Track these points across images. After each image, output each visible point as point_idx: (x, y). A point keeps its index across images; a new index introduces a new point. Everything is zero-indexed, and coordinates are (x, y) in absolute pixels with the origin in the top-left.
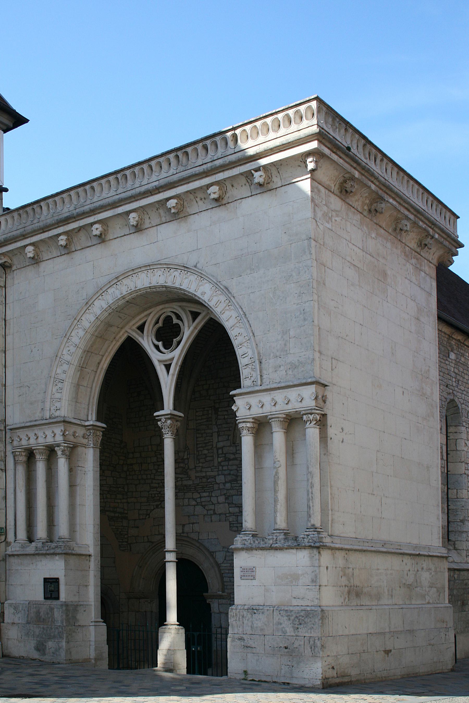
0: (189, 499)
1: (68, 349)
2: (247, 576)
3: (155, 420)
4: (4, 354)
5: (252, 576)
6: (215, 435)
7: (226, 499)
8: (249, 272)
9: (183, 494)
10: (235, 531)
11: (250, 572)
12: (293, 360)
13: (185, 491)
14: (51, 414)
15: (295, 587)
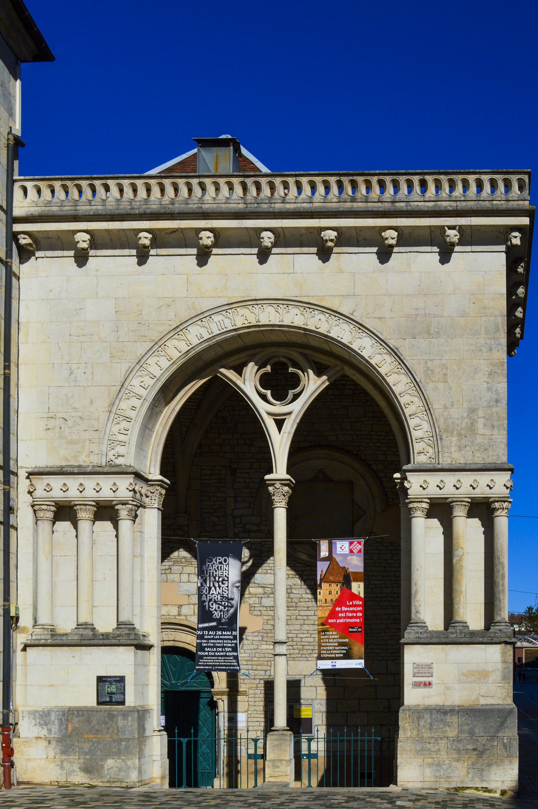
0: (189, 574)
1: (141, 379)
2: (422, 673)
3: (264, 485)
4: (17, 369)
5: (429, 673)
8: (427, 336)
9: (180, 567)
10: (257, 616)
11: (426, 669)
12: (482, 442)
13: (183, 565)
14: (108, 460)
15: (484, 684)
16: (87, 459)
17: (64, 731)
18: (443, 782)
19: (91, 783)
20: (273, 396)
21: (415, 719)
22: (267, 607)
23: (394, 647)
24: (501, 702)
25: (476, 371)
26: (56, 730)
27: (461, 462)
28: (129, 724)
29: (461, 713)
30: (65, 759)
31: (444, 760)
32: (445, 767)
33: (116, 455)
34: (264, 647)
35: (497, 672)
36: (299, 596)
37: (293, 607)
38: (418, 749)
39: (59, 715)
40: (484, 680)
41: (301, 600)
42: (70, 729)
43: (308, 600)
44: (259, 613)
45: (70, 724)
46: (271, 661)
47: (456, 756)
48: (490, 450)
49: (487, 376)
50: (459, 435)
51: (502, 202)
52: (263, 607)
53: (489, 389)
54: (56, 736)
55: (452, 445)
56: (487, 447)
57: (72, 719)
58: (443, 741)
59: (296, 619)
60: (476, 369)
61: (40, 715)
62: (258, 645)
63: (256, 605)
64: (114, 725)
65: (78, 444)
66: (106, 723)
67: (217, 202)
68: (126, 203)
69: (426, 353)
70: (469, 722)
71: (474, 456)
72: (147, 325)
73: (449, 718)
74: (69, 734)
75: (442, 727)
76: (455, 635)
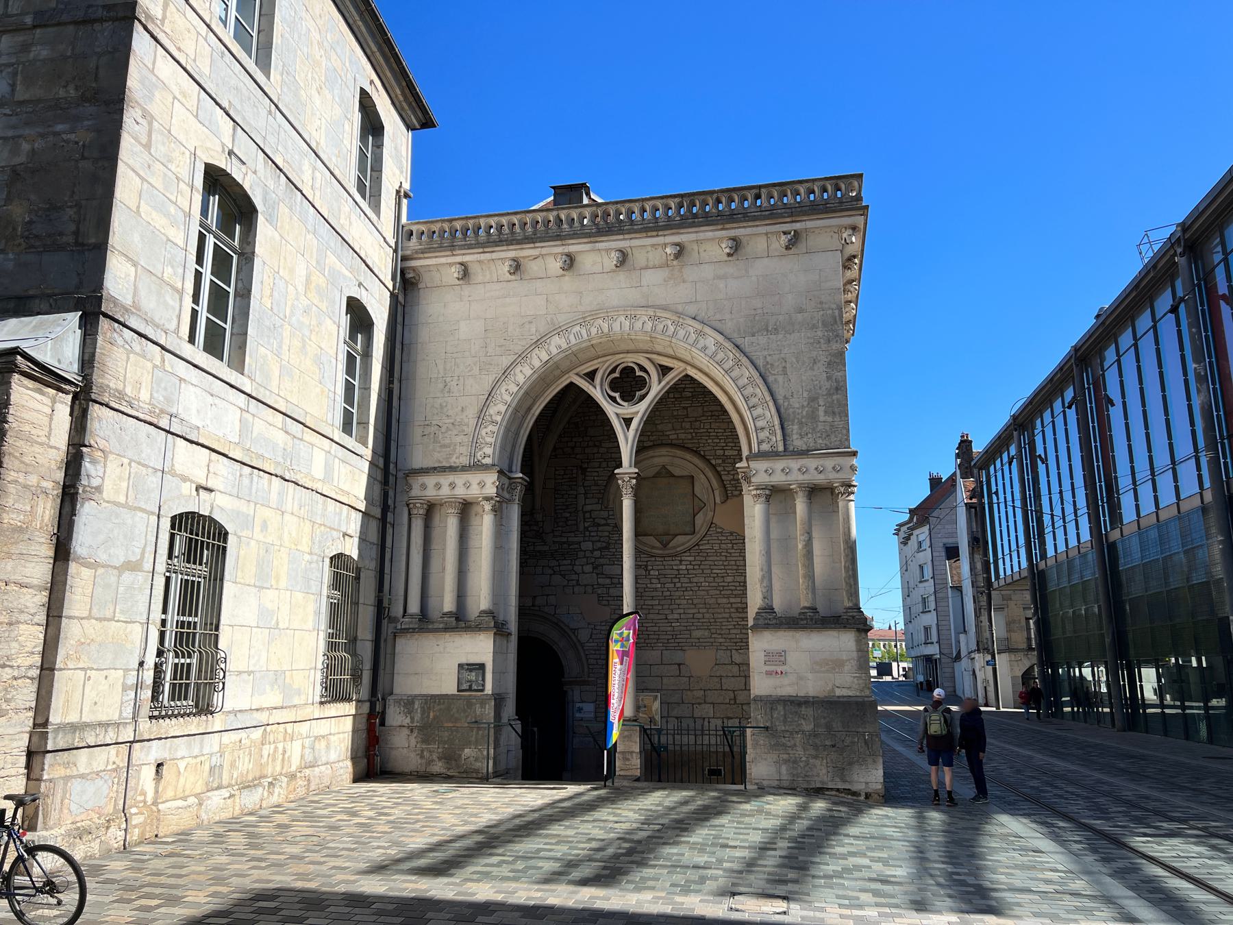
6: (581, 498)
8: (765, 333)
16: (457, 461)
24: (858, 694)
32: (802, 764)
36: (644, 586)
47: (813, 752)
50: (801, 423)
53: (829, 378)
57: (434, 708)
66: (465, 711)
70: (825, 715)
73: (803, 710)
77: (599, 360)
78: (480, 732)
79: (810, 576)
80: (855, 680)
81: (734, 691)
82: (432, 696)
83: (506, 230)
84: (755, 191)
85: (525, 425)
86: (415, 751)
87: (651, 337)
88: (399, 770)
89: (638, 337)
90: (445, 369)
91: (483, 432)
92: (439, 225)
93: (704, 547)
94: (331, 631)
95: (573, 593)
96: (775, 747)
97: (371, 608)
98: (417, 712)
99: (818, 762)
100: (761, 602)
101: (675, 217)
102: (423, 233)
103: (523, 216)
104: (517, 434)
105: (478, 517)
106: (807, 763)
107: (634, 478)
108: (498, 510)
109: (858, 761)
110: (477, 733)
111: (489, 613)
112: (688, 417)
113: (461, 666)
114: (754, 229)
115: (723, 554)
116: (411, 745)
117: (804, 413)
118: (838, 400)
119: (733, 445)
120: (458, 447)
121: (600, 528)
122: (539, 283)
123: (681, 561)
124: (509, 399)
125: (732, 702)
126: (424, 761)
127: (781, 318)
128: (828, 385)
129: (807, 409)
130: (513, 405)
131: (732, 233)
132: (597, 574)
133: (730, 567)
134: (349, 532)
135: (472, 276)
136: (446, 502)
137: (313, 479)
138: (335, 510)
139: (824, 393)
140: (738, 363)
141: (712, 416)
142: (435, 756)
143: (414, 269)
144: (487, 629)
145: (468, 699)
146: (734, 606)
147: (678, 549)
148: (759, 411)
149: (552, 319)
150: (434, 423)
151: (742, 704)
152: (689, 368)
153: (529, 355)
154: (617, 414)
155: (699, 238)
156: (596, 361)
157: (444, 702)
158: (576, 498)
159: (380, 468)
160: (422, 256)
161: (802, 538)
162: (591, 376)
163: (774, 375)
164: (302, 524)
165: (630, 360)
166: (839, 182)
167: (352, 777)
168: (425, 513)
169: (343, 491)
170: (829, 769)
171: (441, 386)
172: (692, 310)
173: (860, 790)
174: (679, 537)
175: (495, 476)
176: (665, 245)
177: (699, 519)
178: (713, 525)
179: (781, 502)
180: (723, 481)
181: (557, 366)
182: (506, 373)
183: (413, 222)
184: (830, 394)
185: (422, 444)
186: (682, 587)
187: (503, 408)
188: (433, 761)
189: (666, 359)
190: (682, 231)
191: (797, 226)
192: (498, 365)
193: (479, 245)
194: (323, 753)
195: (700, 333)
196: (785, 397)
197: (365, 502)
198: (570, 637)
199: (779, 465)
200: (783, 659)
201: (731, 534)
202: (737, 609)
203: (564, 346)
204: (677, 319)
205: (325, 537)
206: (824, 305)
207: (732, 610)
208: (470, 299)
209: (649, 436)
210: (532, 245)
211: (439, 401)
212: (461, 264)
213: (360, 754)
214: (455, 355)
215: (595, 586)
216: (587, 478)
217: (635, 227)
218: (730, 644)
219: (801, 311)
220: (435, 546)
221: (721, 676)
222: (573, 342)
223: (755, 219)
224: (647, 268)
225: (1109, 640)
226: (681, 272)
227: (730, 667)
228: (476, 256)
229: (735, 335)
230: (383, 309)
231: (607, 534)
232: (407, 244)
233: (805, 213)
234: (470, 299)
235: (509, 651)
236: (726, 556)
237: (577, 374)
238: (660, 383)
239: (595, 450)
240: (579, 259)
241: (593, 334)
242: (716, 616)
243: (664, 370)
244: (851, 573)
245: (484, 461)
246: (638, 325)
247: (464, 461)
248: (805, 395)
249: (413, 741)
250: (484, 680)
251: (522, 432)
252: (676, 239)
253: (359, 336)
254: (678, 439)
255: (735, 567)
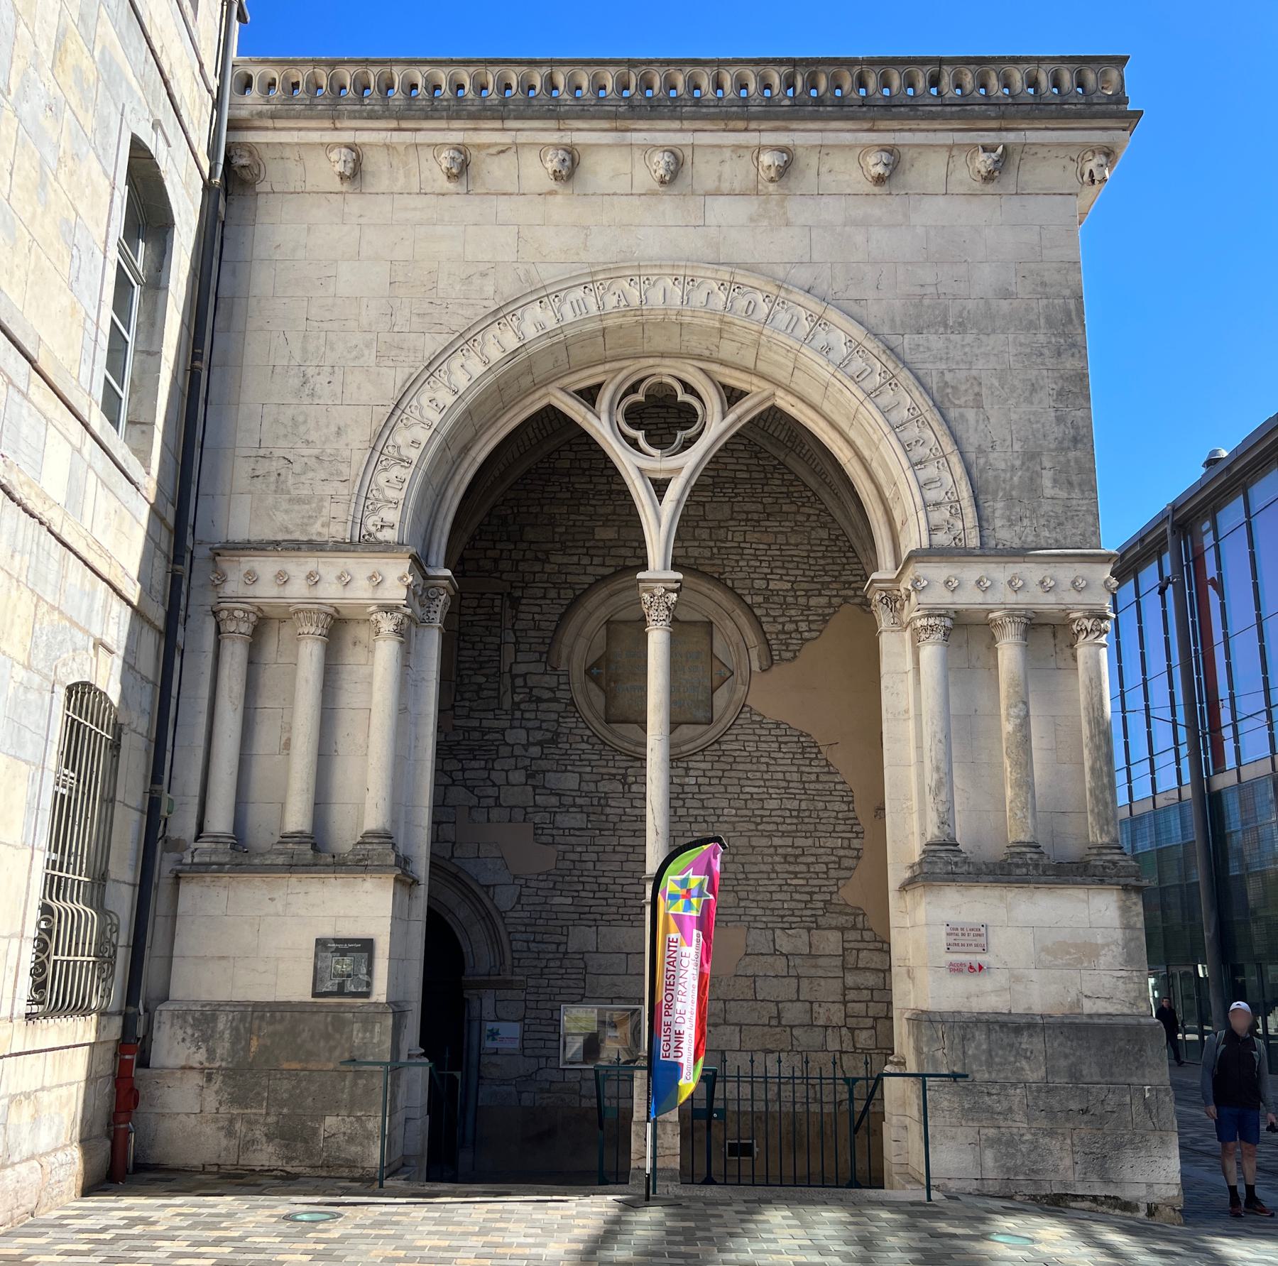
2: (963, 945)
6: (509, 651)
7: (528, 777)
8: (941, 330)
16: (325, 531)
17: (242, 1053)
18: (1023, 1182)
19: (289, 1169)
20: (648, 437)
21: (957, 1041)
22: (564, 829)
23: (786, 906)
24: (1126, 1011)
25: (1034, 389)
26: (225, 1051)
27: (1014, 546)
28: (375, 1041)
29: (1051, 1032)
30: (238, 1114)
31: (1022, 1132)
32: (1024, 1148)
33: (380, 524)
34: (557, 900)
35: (1113, 947)
36: (620, 811)
37: (609, 830)
38: (967, 1106)
39: (233, 1019)
40: (1090, 962)
41: (623, 818)
42: (253, 1050)
43: (635, 818)
44: (550, 839)
45: (255, 1038)
46: (568, 927)
47: (1045, 1124)
48: (1068, 526)
49: (1055, 397)
50: (1010, 498)
51: (1079, 106)
52: (559, 828)
53: (1060, 420)
54: (224, 1064)
55: (996, 515)
56: (1062, 519)
57: (260, 1028)
58: (1018, 1091)
59: (614, 851)
60: (1033, 385)
61: (194, 1018)
62: (546, 897)
63: (545, 826)
64: (343, 1041)
65: (309, 503)
66: (328, 1037)
67: (582, 103)
68: (424, 103)
69: (941, 359)
70: (1067, 1051)
71: (1037, 536)
72: (445, 305)
73: (1025, 1041)
74: (250, 1060)
75: (1012, 1059)
76: (1024, 870)
77: (607, 366)
78: (361, 1082)
79: (1026, 783)
80: (1120, 983)
81: (777, 1003)
82: (256, 1005)
83: (445, 91)
84: (930, 69)
85: (457, 478)
86: (216, 1121)
87: (721, 321)
88: (172, 1162)
89: (696, 321)
90: (304, 350)
91: (381, 479)
92: (308, 70)
93: (729, 747)
94: (53, 856)
95: (489, 820)
96: (969, 1114)
97: (136, 816)
98: (221, 1037)
99: (1055, 1144)
100: (936, 832)
101: (781, 100)
102: (272, 84)
103: (481, 69)
104: (441, 496)
105: (359, 649)
106: (1035, 1146)
107: (673, 591)
108: (405, 634)
109: (1131, 1142)
110: (355, 1084)
111: (385, 836)
112: (706, 520)
113: (321, 944)
114: (931, 135)
115: (763, 760)
116: (207, 1109)
117: (1016, 479)
118: (1077, 461)
119: (784, 572)
120: (326, 504)
121: (543, 706)
122: (503, 203)
123: (687, 769)
124: (436, 418)
125: (774, 1022)
126: (234, 1142)
127: (970, 305)
128: (1058, 431)
129: (1020, 473)
130: (444, 431)
131: (888, 138)
132: (535, 787)
133: (774, 783)
134: (107, 640)
135: (368, 178)
136: (297, 612)
137: (45, 498)
138: (82, 584)
139: (1052, 446)
140: (891, 381)
141: (747, 520)
142: (258, 1133)
143: (250, 148)
144: (380, 869)
145: (336, 1011)
146: (780, 851)
147: (684, 748)
148: (930, 471)
149: (527, 271)
150: (277, 453)
151: (792, 1027)
152: (780, 393)
153: (479, 337)
154: (640, 470)
155: (825, 142)
156: (600, 369)
157: (282, 1019)
158: (499, 649)
159: (166, 526)
160: (269, 123)
161: (1014, 711)
162: (589, 395)
163: (960, 407)
164: (14, 593)
165: (667, 371)
166: (1084, 67)
167: (80, 1183)
168: (249, 631)
169: (100, 547)
170: (1078, 1158)
171: (295, 382)
172: (803, 275)
173: (1138, 1200)
174: (684, 727)
175: (406, 564)
176: (761, 148)
177: (720, 698)
178: (746, 709)
179: (960, 647)
180: (765, 633)
181: (529, 366)
182: (432, 366)
183: (254, 58)
184: (1062, 449)
185: (250, 492)
186: (688, 815)
187: (423, 435)
188: (253, 1141)
189: (737, 374)
190: (794, 125)
191: (1011, 137)
192: (415, 351)
193: (387, 113)
194: (25, 1130)
195: (819, 321)
196: (980, 450)
197: (139, 586)
198: (480, 901)
199: (971, 572)
200: (982, 940)
201: (778, 725)
202: (785, 856)
203: (551, 324)
204: (775, 291)
205: (60, 638)
206: (1047, 290)
207: (777, 859)
208: (362, 221)
209: (635, 548)
210: (498, 124)
211: (290, 412)
212: (351, 147)
213: (97, 1130)
214: (326, 326)
215: (529, 810)
216: (522, 616)
217: (704, 110)
218: (770, 919)
219: (1006, 294)
220: (268, 702)
221: (755, 976)
222: (569, 317)
223: (932, 117)
224: (717, 193)
225: (1211, 935)
226: (783, 207)
227: (770, 959)
228: (384, 134)
229: (885, 330)
230: (192, 208)
231: (554, 716)
232: (241, 100)
233: (1027, 117)
234: (362, 221)
235: (413, 917)
236: (767, 764)
237: (563, 389)
238: (724, 418)
239: (537, 568)
240: (587, 162)
241: (609, 308)
242: (748, 868)
243: (732, 396)
244: (1106, 780)
245: (381, 536)
246: (699, 297)
247: (339, 531)
248: (1017, 447)
249: (211, 1101)
250: (370, 973)
251: (450, 491)
252: (783, 139)
253: (142, 245)
254: (687, 557)
255: (784, 784)
